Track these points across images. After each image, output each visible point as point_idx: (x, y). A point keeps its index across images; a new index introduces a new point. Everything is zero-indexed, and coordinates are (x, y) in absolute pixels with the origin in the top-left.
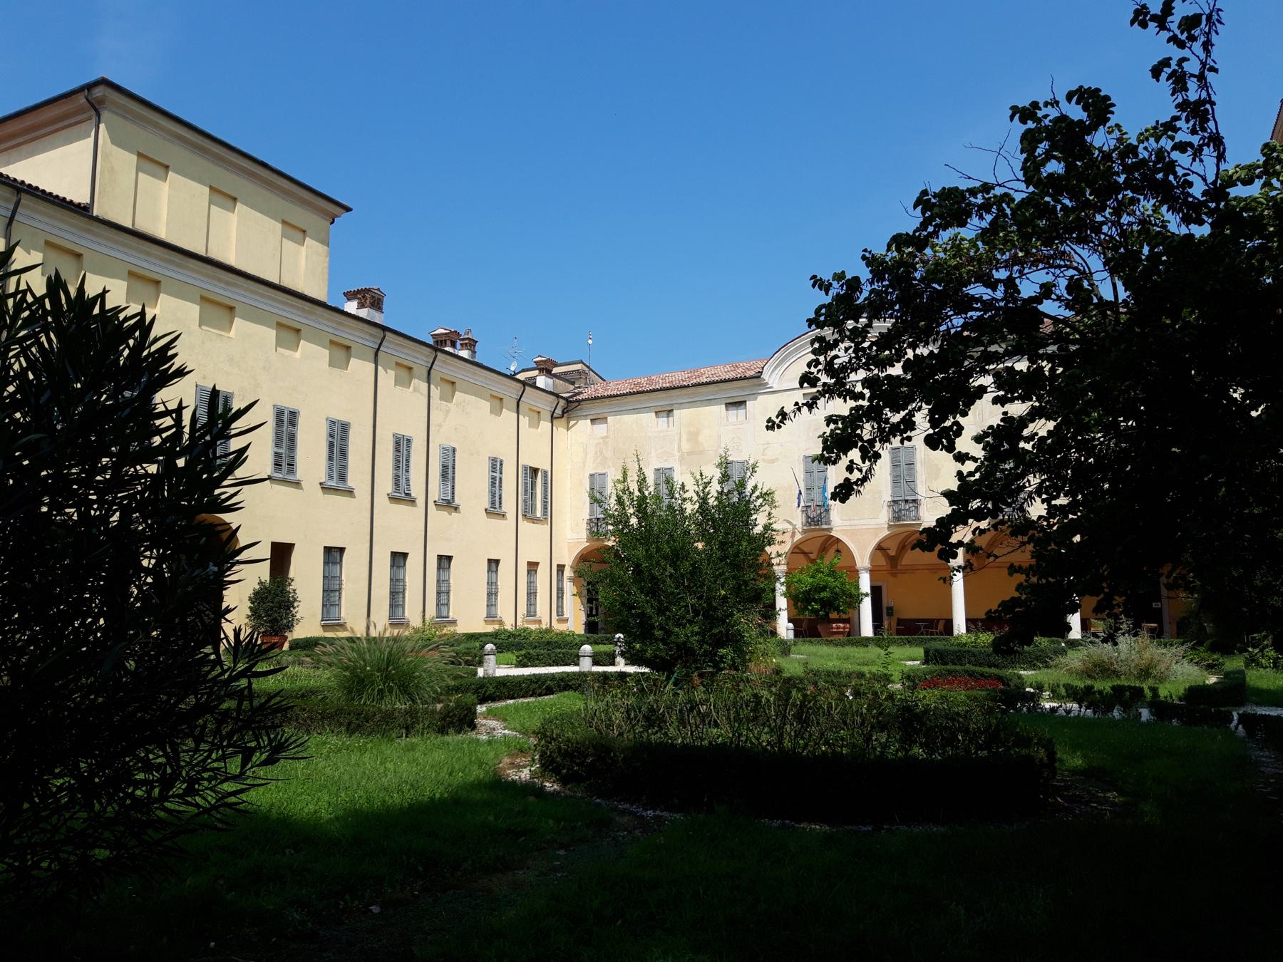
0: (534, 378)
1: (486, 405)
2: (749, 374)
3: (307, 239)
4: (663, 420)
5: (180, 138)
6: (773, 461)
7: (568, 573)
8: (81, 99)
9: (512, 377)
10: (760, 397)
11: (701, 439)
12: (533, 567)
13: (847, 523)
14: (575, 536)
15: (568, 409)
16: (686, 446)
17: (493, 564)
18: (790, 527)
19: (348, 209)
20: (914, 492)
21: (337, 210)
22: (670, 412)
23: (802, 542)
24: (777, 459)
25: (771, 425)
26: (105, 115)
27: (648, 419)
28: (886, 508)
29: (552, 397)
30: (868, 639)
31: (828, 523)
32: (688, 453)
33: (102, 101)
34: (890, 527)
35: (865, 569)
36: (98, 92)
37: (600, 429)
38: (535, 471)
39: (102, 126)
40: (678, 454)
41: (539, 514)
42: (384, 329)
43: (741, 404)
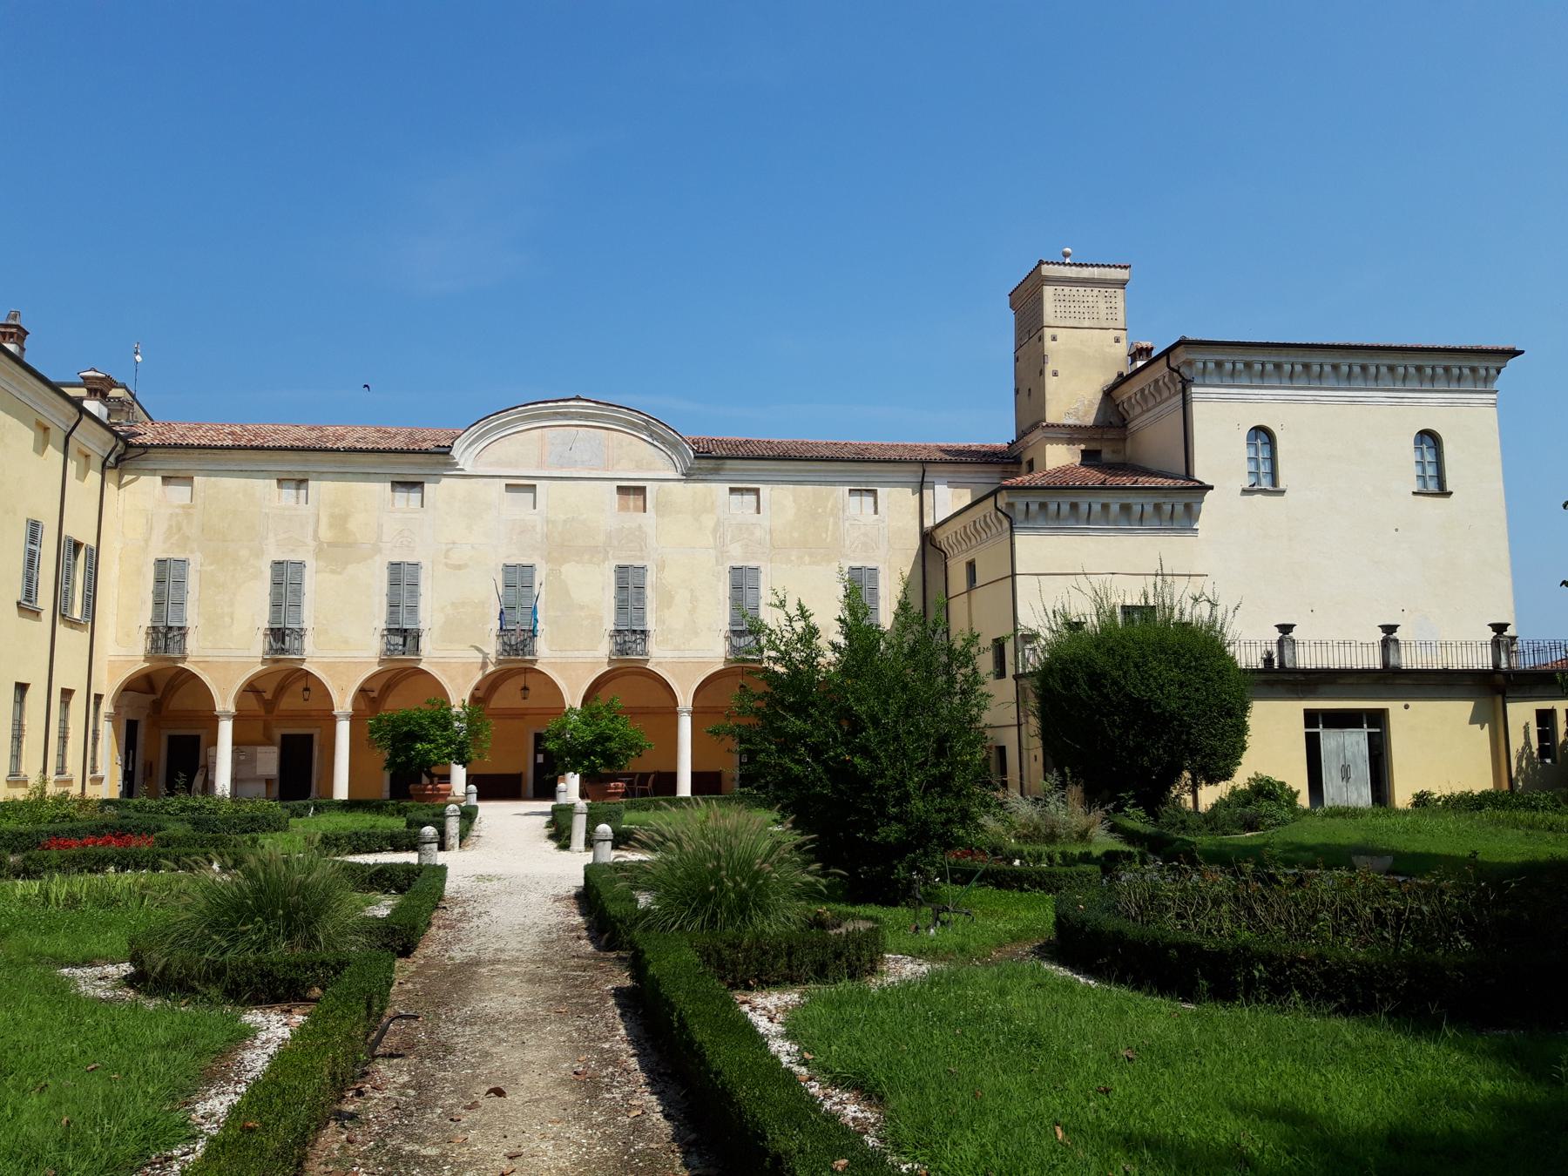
0: (82, 399)
1: (29, 436)
4: (289, 494)
6: (459, 567)
7: (106, 707)
9: (56, 388)
10: (445, 481)
11: (352, 525)
12: (67, 694)
13: (559, 654)
14: (123, 651)
15: (125, 456)
16: (325, 534)
17: (22, 688)
18: (479, 658)
20: (642, 619)
22: (301, 483)
23: (258, 677)
24: (466, 566)
27: (265, 488)
28: (607, 638)
29: (108, 435)
30: (687, 799)
31: (532, 653)
32: (329, 544)
34: (611, 661)
35: (227, 716)
37: (179, 493)
38: (77, 546)
40: (312, 544)
41: (77, 615)
43: (416, 485)
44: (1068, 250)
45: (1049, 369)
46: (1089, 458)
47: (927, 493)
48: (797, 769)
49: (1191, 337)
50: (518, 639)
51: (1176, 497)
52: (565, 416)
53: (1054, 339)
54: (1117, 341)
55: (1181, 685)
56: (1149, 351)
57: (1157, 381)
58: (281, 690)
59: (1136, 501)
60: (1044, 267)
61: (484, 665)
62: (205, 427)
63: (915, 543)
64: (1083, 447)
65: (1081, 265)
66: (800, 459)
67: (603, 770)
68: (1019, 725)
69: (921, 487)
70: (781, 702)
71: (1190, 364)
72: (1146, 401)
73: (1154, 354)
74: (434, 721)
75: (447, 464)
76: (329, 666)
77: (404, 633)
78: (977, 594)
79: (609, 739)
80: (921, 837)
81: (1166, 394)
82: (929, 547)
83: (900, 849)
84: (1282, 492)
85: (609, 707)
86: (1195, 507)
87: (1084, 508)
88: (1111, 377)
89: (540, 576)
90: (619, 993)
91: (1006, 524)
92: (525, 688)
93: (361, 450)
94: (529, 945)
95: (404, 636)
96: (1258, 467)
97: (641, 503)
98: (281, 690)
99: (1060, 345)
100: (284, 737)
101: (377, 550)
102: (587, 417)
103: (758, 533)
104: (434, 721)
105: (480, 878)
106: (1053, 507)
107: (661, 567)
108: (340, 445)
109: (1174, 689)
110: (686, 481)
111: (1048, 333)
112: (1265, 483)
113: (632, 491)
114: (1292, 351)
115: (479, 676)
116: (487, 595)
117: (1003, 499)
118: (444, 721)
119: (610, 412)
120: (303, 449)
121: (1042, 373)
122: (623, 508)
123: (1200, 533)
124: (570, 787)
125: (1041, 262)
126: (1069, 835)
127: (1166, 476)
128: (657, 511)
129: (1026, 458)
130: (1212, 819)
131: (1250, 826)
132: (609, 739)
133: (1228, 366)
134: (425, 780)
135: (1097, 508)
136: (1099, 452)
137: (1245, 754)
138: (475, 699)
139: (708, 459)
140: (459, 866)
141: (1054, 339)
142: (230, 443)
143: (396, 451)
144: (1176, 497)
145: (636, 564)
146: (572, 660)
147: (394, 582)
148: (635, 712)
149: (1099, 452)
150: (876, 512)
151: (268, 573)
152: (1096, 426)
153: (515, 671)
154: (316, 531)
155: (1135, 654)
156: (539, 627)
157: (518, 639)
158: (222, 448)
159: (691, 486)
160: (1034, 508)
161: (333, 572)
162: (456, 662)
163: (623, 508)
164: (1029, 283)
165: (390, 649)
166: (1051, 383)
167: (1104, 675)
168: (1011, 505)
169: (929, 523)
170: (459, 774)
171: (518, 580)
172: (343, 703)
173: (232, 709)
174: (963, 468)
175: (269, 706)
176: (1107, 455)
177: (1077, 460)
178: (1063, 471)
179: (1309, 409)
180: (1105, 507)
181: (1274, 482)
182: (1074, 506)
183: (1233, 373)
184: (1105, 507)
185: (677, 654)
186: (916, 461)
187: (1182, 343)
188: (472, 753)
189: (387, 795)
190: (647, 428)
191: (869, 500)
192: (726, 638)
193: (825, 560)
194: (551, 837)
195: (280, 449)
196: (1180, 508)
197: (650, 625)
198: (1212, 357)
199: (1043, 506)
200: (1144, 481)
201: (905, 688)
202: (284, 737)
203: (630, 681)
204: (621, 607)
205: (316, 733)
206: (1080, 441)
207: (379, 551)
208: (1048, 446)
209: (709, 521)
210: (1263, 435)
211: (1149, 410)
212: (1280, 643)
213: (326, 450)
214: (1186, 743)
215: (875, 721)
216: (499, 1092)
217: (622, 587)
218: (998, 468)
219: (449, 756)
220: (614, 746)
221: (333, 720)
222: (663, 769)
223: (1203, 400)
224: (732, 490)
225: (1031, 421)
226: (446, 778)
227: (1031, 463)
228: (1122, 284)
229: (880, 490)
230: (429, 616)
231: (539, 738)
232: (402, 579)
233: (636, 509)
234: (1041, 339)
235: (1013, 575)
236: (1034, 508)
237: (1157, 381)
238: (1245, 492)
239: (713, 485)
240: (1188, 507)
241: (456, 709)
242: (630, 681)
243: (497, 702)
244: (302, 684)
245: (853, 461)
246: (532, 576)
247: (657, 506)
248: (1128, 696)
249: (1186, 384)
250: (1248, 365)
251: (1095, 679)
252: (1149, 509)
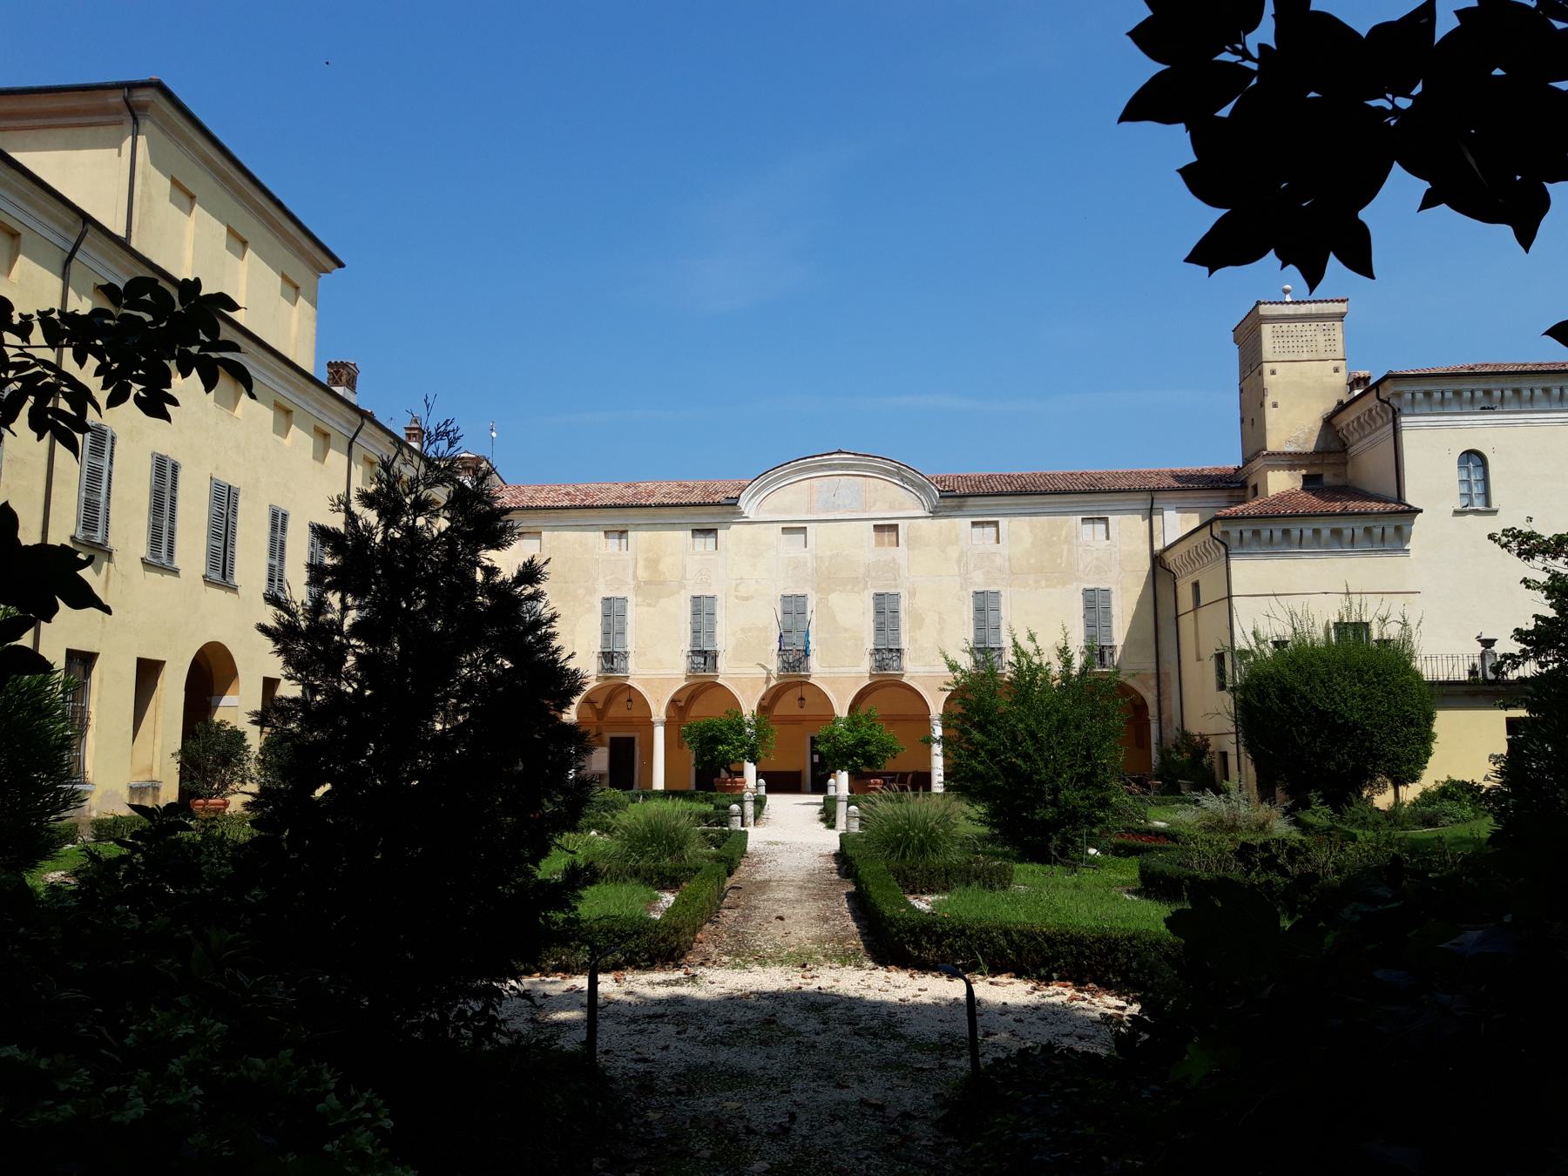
2: (719, 498)
3: (21, 258)
4: (613, 543)
5: (207, 162)
6: (747, 599)
8: (115, 99)
11: (662, 567)
16: (642, 574)
19: (341, 265)
20: (897, 639)
21: (327, 263)
22: (622, 533)
25: (1525, 581)
26: (146, 125)
33: (144, 107)
34: (871, 675)
36: (142, 96)
39: (142, 140)
42: (365, 416)
43: (710, 532)
44: (1288, 287)
45: (1268, 401)
46: (1311, 483)
47: (1155, 518)
48: (980, 768)
49: (1397, 370)
50: (795, 658)
51: (1383, 518)
52: (830, 467)
53: (1273, 373)
54: (1336, 370)
55: (1364, 698)
56: (1366, 380)
57: (1370, 411)
58: (609, 700)
59: (1346, 526)
60: (1262, 307)
61: (768, 680)
62: (547, 488)
63: (1145, 565)
64: (1304, 472)
65: (1298, 303)
66: (1041, 493)
67: (866, 769)
69: (1150, 513)
70: (970, 720)
71: (1399, 395)
72: (1363, 428)
73: (1372, 382)
74: (731, 728)
76: (647, 682)
77: (704, 653)
78: (1201, 611)
79: (868, 743)
80: (1071, 817)
81: (1379, 422)
82: (1159, 569)
83: (1054, 825)
84: (1496, 512)
85: (868, 717)
86: (1405, 529)
87: (1295, 533)
88: (1331, 406)
89: (811, 605)
90: (848, 895)
91: (1223, 550)
92: (802, 699)
93: (668, 505)
94: (801, 875)
95: (704, 656)
96: (1470, 488)
98: (609, 700)
99: (1279, 379)
100: (612, 739)
101: (682, 586)
102: (848, 467)
103: (999, 561)
104: (731, 728)
105: (770, 843)
106: (1265, 534)
107: (912, 594)
108: (651, 501)
109: (1357, 701)
111: (1267, 367)
112: (1478, 504)
113: (887, 529)
114: (1502, 379)
115: (764, 690)
116: (767, 621)
117: (1218, 529)
118: (738, 727)
119: (868, 461)
120: (623, 506)
121: (1262, 405)
122: (879, 544)
123: (1412, 553)
124: (841, 783)
125: (1258, 303)
126: (1249, 828)
127: (1379, 499)
129: (1251, 482)
130: (1393, 816)
131: (1429, 822)
132: (868, 743)
133: (1437, 396)
134: (724, 774)
135: (1308, 533)
136: (1321, 476)
137: (1431, 759)
138: (761, 708)
139: (953, 498)
140: (757, 837)
141: (1273, 373)
142: (566, 503)
143: (695, 505)
144: (1383, 518)
146: (840, 675)
147: (696, 613)
148: (892, 720)
149: (1321, 476)
151: (599, 607)
152: (1316, 453)
153: (792, 682)
154: (635, 573)
155: (1322, 670)
156: (812, 647)
157: (795, 658)
158: (562, 508)
159: (937, 522)
160: (1247, 535)
161: (649, 605)
162: (746, 677)
163: (879, 544)
164: (1249, 321)
165: (693, 668)
166: (1271, 415)
167: (1293, 690)
168: (1226, 533)
169: (1158, 546)
170: (750, 770)
171: (794, 607)
172: (659, 712)
174: (1189, 494)
175: (600, 714)
176: (1328, 479)
177: (1299, 485)
178: (1280, 498)
179: (1523, 431)
180: (1317, 532)
181: (1488, 502)
182: (1286, 532)
183: (1443, 402)
184: (1317, 532)
186: (1145, 490)
188: (761, 754)
189: (693, 787)
191: (1101, 527)
193: (1051, 593)
194: (822, 820)
195: (606, 507)
196: (1390, 531)
197: (905, 644)
198: (1419, 388)
199: (1256, 533)
200: (1354, 506)
201: (1057, 711)
202: (612, 739)
203: (886, 690)
204: (879, 629)
205: (636, 735)
206: (1301, 467)
207: (684, 587)
208: (1270, 474)
209: (953, 552)
210: (1474, 459)
211: (1377, 429)
212: (1483, 656)
213: (641, 506)
214: (1369, 750)
215: (1033, 735)
216: (781, 918)
217: (879, 612)
218: (1226, 493)
219: (743, 755)
220: (872, 749)
221: (651, 725)
222: (921, 770)
223: (1412, 428)
224: (974, 524)
225: (1254, 448)
226: (741, 774)
227: (1255, 488)
228: (1340, 317)
229: (1111, 518)
230: (724, 640)
231: (813, 741)
232: (702, 609)
234: (1260, 373)
235: (1230, 597)
236: (1247, 535)
237: (1370, 411)
238: (1457, 513)
240: (1398, 529)
241: (748, 717)
242: (886, 690)
243: (781, 709)
244: (625, 697)
245: (1085, 492)
246: (805, 605)
248: (1315, 708)
249: (1396, 414)
250: (1458, 394)
251: (1286, 693)
252: (1359, 532)
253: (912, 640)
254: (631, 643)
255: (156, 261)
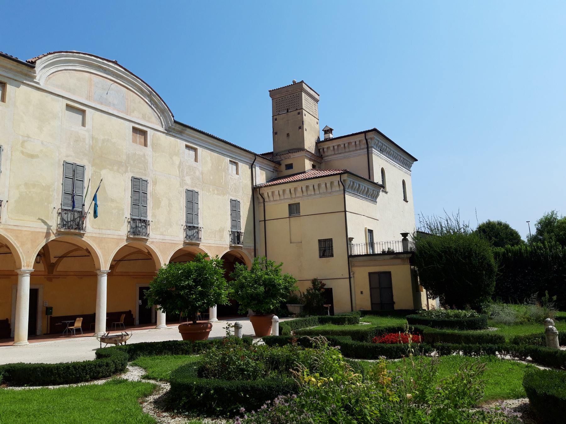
10: (23, 87)
13: (98, 231)
18: (44, 229)
28: (126, 223)
34: (128, 239)
52: (105, 70)
61: (48, 234)
68: (350, 278)
69: (252, 167)
75: (26, 75)
89: (88, 174)
91: (342, 188)
97: (143, 140)
107: (155, 183)
110: (167, 134)
122: (134, 141)
128: (153, 148)
145: (144, 178)
150: (237, 173)
171: (73, 174)
173: (31, 268)
185: (162, 237)
187: (375, 130)
190: (149, 96)
192: (185, 230)
209: (177, 160)
230: (204, 221)
233: (140, 144)
239: (179, 140)
247: (153, 145)
253: (154, 216)
254: (201, 223)
255: (362, 131)
